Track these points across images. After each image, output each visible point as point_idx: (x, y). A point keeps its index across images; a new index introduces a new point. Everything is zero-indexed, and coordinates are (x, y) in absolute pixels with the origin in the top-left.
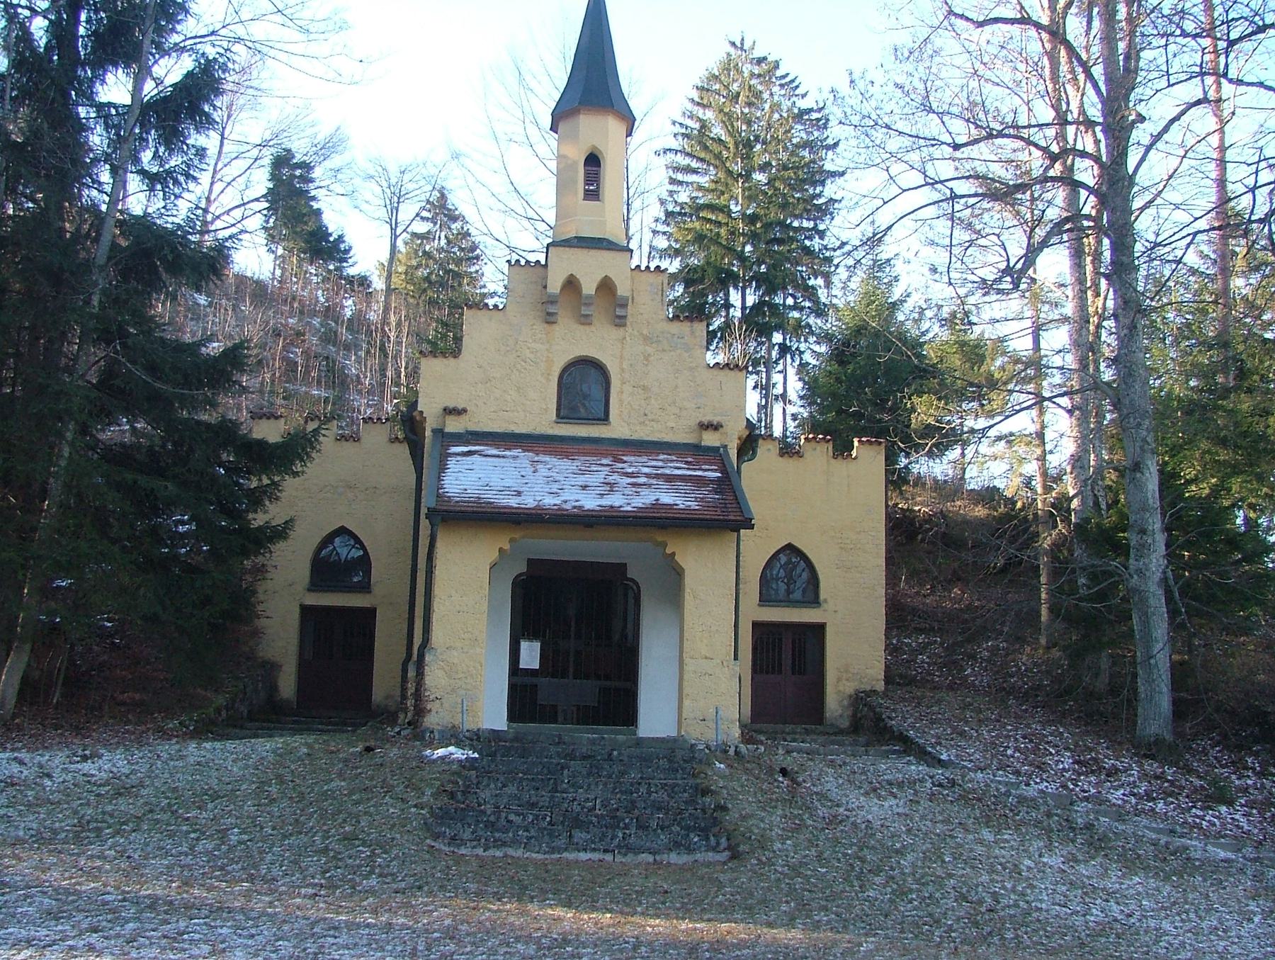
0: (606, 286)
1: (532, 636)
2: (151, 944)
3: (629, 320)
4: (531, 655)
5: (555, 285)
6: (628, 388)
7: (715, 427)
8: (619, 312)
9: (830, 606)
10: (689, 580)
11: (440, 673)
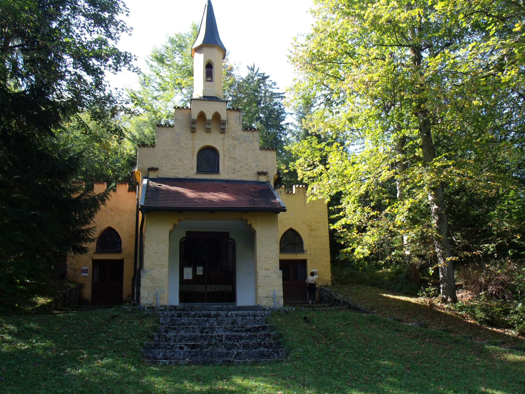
0: (217, 116)
1: (188, 266)
2: (171, 363)
3: (226, 130)
4: (188, 273)
5: (195, 116)
6: (226, 158)
7: (264, 174)
8: (222, 127)
9: (308, 252)
10: (258, 235)
11: (148, 281)
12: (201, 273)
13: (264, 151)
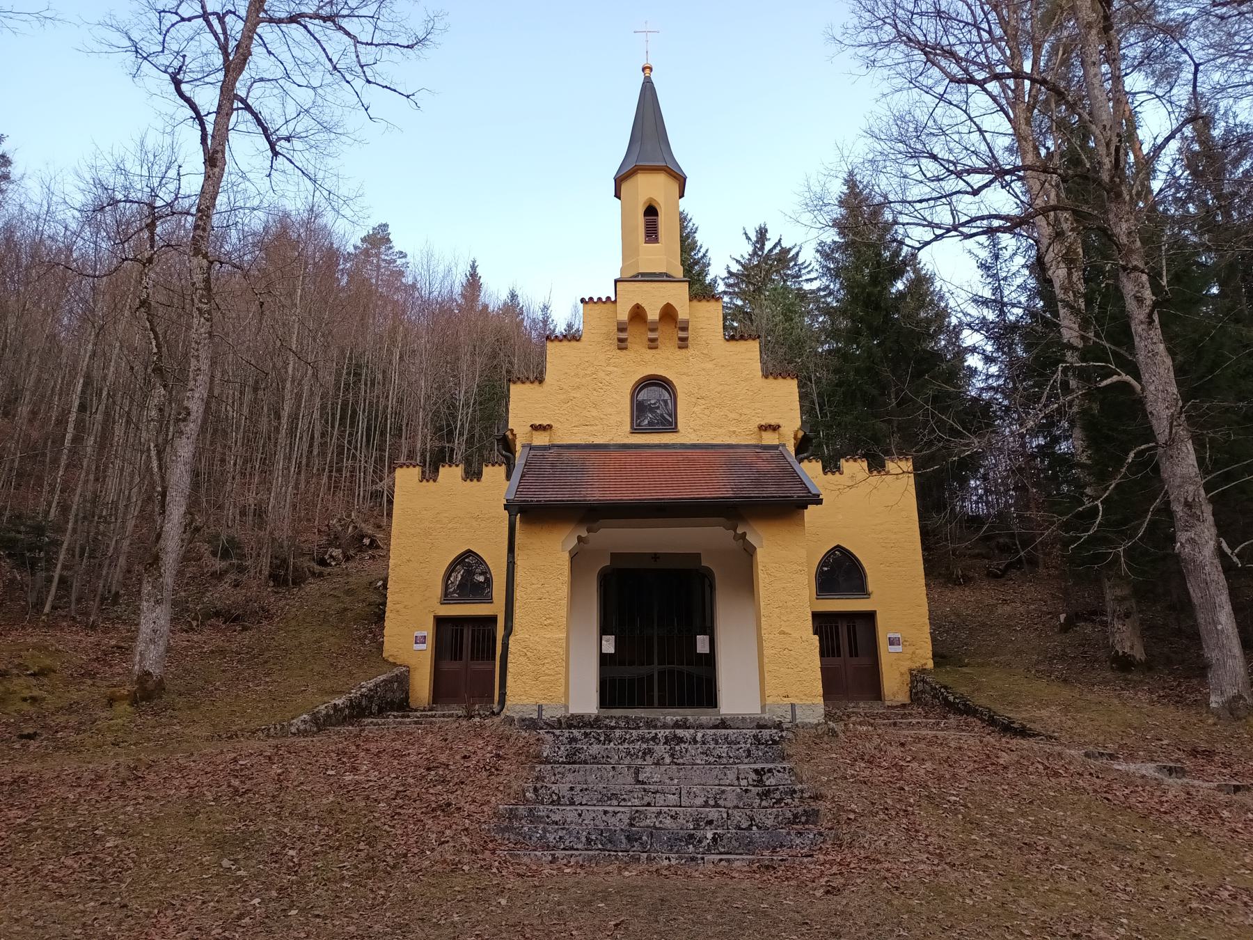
0: (668, 313)
5: (624, 316)
7: (775, 428)
8: (682, 334)
9: (616, 337)
10: (761, 556)
12: (612, 651)
13: (733, 343)
